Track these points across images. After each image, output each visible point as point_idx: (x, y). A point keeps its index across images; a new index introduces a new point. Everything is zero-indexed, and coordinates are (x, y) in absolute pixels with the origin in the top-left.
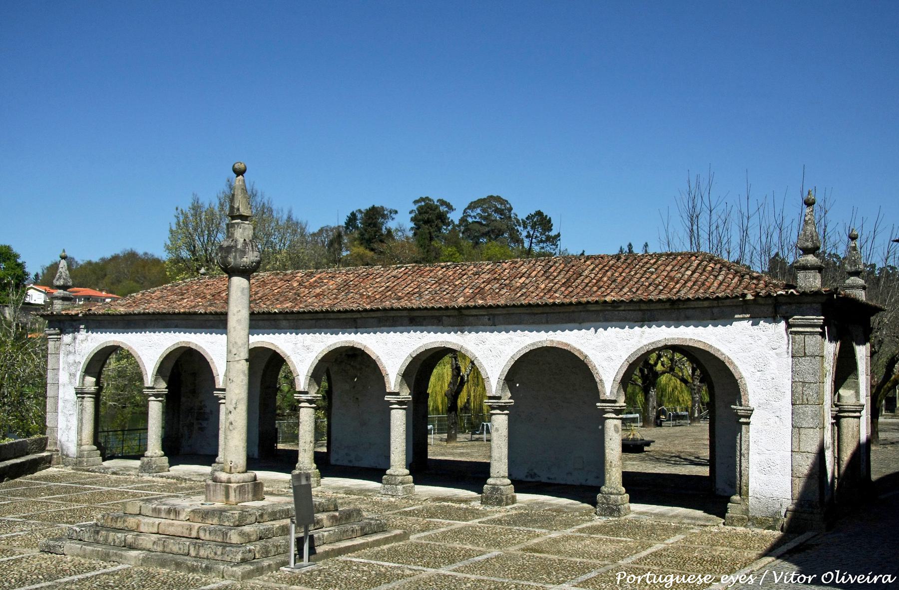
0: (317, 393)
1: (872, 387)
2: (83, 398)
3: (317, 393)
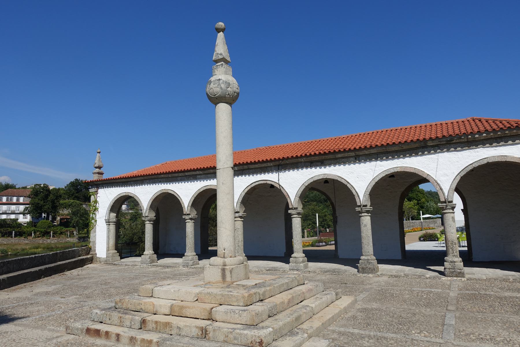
0: (244, 212)
2: (109, 225)
3: (244, 212)
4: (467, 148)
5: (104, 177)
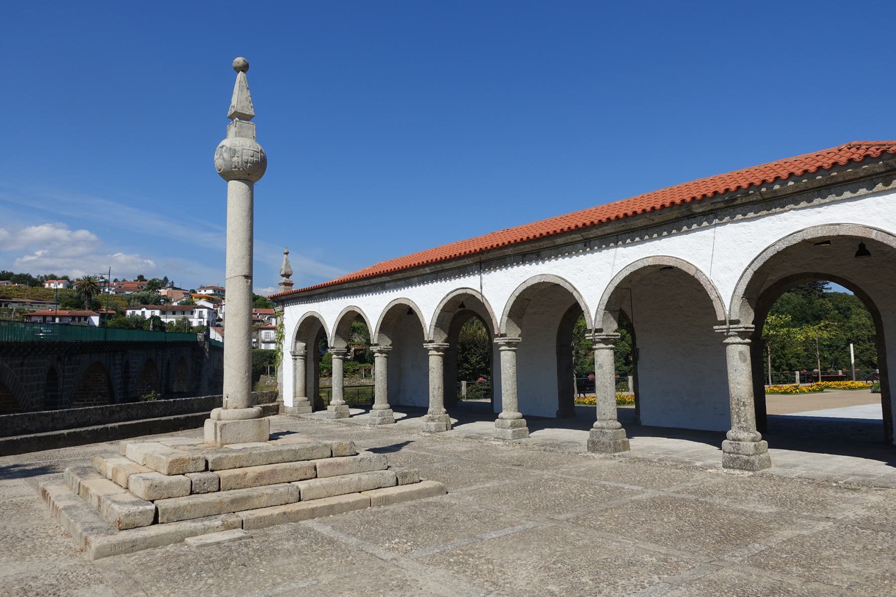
0: (446, 341)
1: (273, 371)
4: (765, 212)
5: (294, 289)
